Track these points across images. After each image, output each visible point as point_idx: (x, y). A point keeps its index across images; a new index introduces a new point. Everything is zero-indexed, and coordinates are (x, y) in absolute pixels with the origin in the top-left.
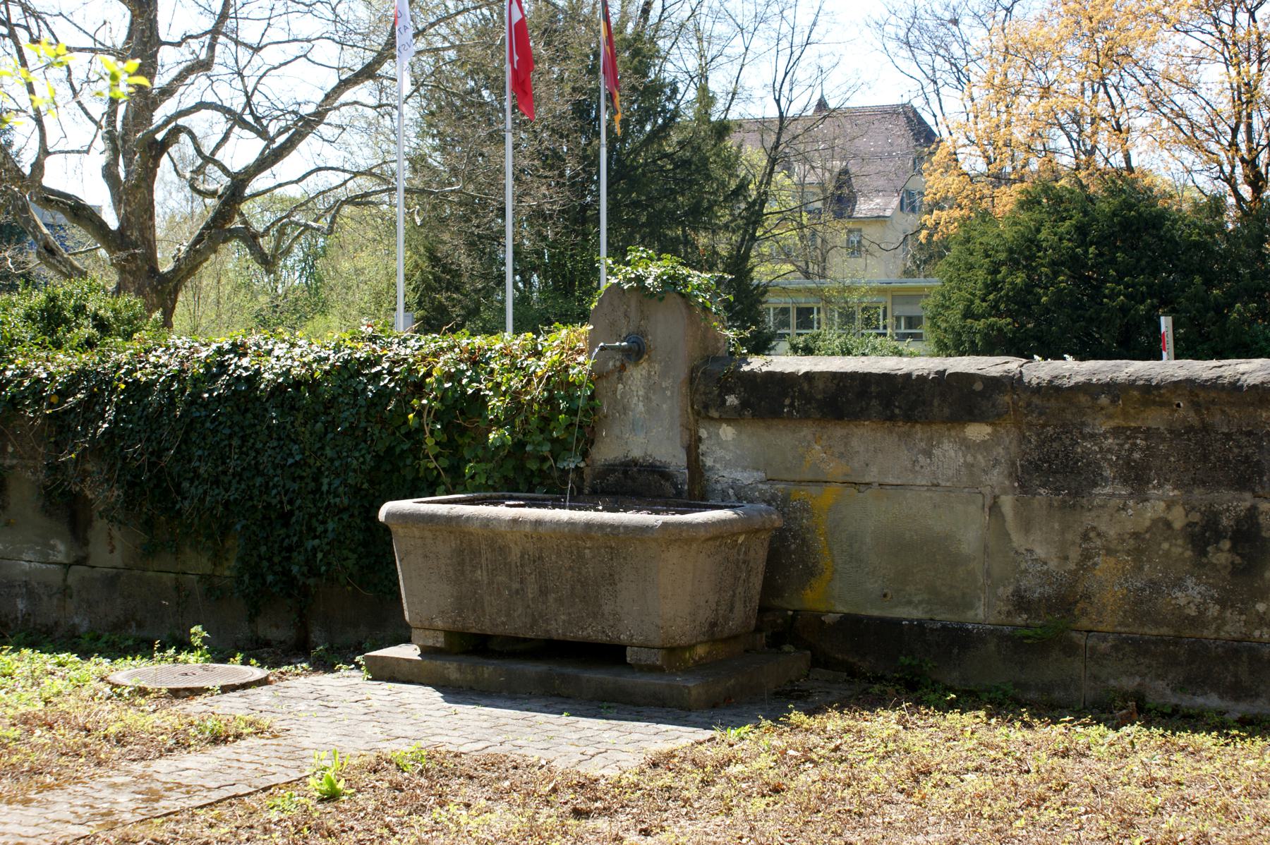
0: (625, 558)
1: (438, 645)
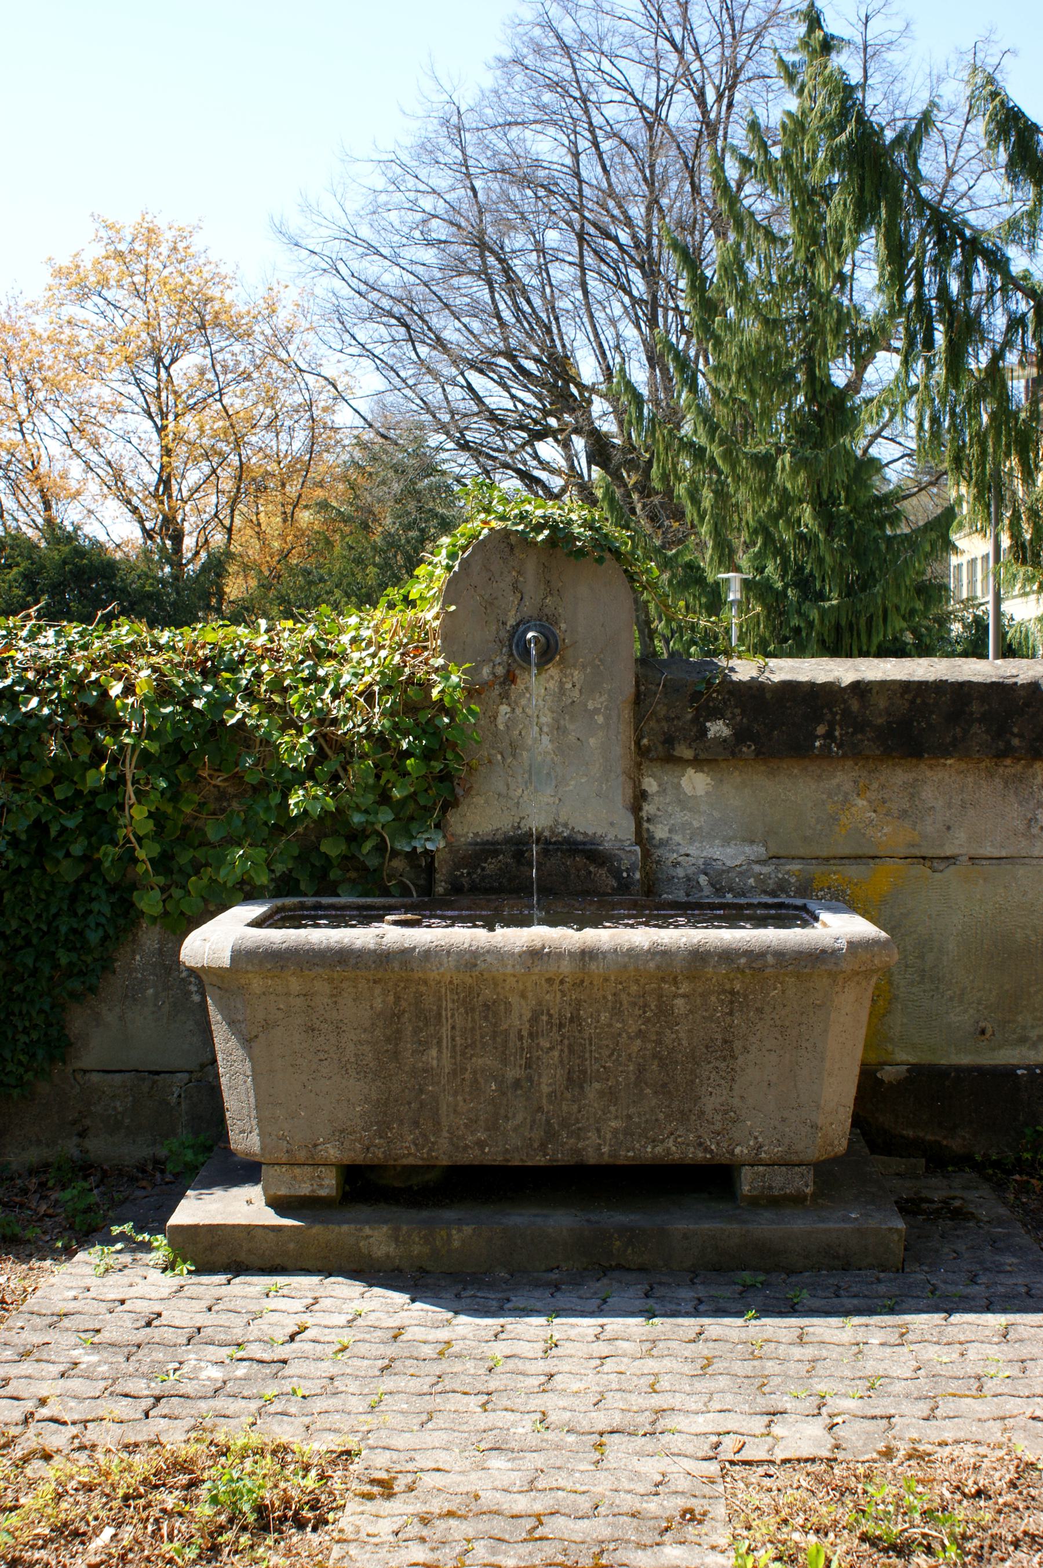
0: (759, 1011)
1: (323, 1193)
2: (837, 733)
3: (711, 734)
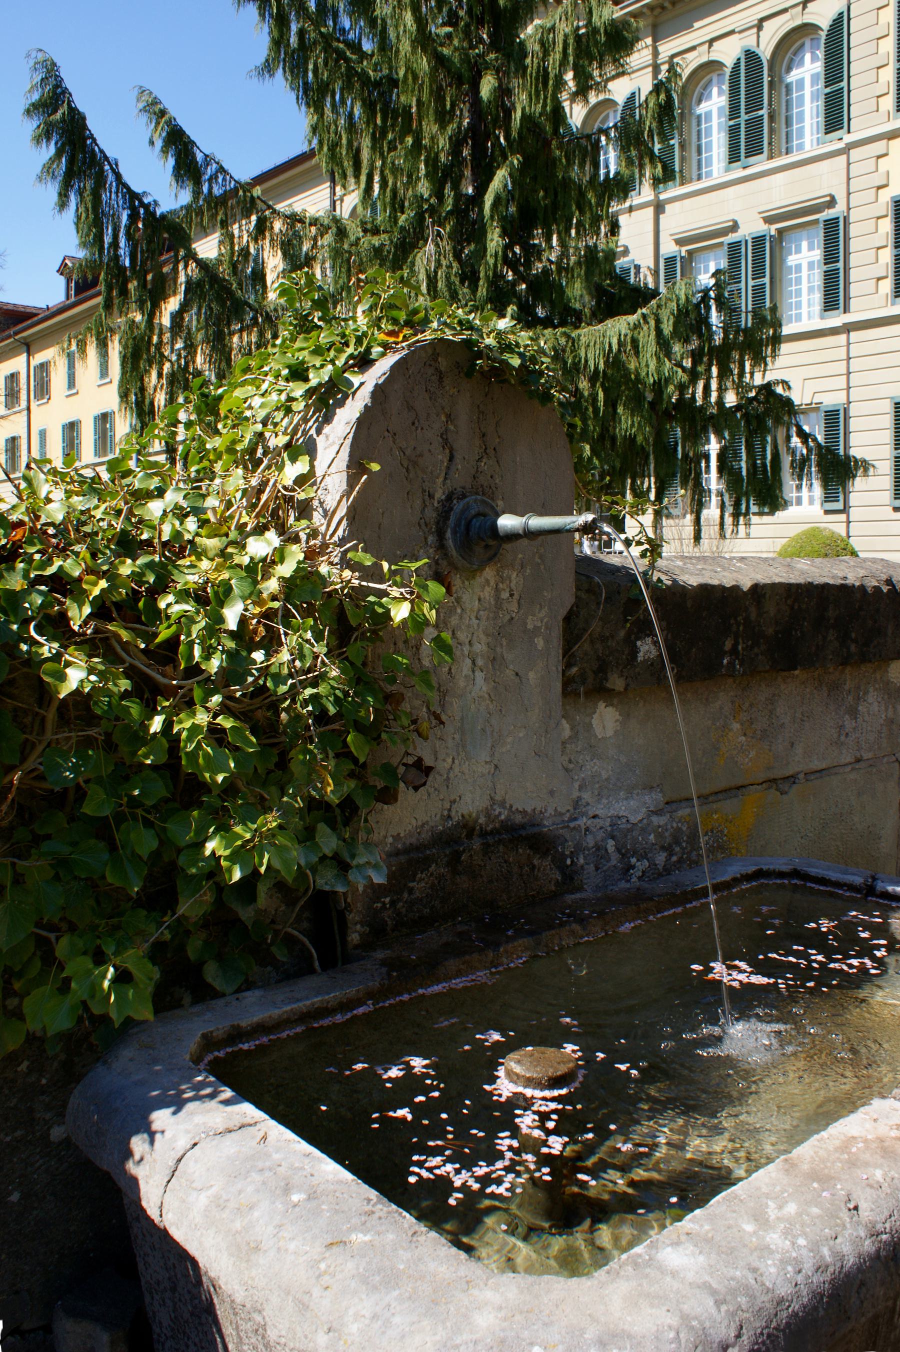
2: (740, 648)
3: (640, 657)
